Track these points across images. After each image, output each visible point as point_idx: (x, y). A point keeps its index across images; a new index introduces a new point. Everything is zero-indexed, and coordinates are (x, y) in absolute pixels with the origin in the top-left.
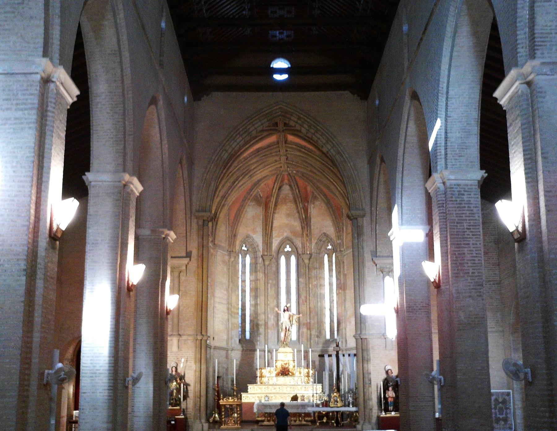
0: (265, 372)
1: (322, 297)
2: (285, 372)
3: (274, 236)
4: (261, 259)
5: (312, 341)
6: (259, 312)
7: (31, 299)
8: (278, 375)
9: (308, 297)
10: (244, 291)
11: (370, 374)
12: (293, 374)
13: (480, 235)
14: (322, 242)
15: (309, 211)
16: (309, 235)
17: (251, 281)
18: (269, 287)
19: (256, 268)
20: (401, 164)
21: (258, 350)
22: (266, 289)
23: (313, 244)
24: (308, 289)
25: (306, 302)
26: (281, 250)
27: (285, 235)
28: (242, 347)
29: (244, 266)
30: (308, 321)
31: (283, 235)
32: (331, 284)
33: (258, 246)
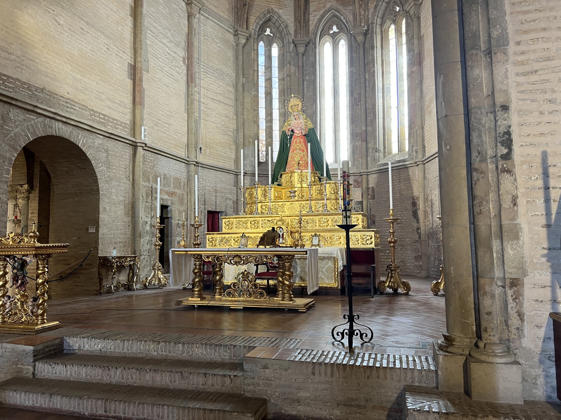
4: (292, 45)
5: (369, 158)
7: (269, 140)
9: (363, 92)
10: (269, 94)
11: (505, 108)
13: (517, 32)
17: (280, 80)
18: (305, 86)
21: (339, 176)
24: (362, 80)
29: (269, 57)
33: (287, 26)
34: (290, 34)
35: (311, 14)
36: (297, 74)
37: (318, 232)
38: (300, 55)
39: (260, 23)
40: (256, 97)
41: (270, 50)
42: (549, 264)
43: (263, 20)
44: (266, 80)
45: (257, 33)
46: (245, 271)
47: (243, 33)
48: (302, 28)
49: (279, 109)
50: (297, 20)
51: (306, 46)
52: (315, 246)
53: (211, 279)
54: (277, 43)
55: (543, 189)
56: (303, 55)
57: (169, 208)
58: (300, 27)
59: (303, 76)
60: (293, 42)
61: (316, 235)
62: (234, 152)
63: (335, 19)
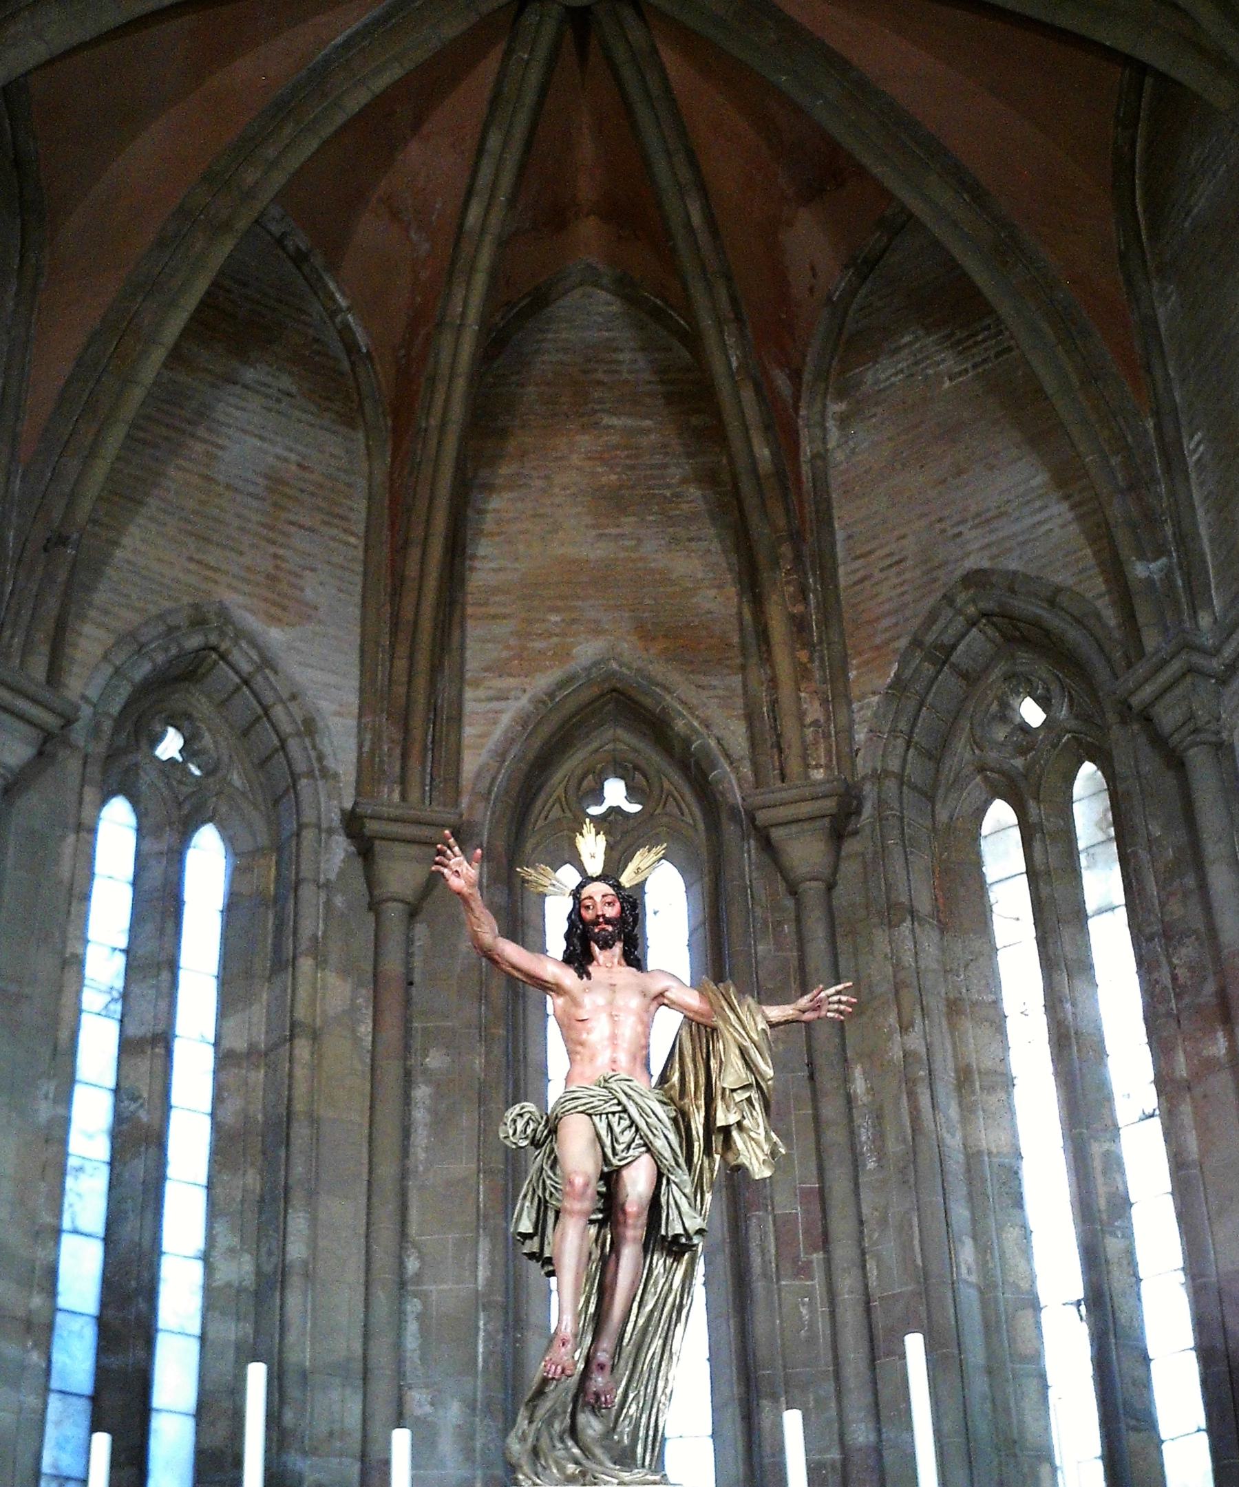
1: (999, 1186)
3: (474, 660)
4: (340, 848)
15: (807, 450)
16: (824, 630)
17: (225, 1059)
18: (420, 1115)
20: (950, 1301)
22: (387, 1133)
23: (866, 709)
25: (825, 1242)
27: (587, 651)
29: (158, 903)
30: (861, 1434)
31: (563, 654)
32: (1074, 1048)
33: (309, 727)
34: (325, 773)
35: (477, 684)
36: (365, 1029)
38: (394, 912)
40: (55, 1135)
41: (176, 857)
42: (149, 1035)
43: (160, 658)
44: (128, 1047)
45: (107, 725)
46: (544, 491)
47: (22, 704)
48: (416, 750)
49: (206, 1258)
50: (376, 698)
54: (222, 829)
55: (1090, 907)
56: (413, 913)
60: (353, 823)
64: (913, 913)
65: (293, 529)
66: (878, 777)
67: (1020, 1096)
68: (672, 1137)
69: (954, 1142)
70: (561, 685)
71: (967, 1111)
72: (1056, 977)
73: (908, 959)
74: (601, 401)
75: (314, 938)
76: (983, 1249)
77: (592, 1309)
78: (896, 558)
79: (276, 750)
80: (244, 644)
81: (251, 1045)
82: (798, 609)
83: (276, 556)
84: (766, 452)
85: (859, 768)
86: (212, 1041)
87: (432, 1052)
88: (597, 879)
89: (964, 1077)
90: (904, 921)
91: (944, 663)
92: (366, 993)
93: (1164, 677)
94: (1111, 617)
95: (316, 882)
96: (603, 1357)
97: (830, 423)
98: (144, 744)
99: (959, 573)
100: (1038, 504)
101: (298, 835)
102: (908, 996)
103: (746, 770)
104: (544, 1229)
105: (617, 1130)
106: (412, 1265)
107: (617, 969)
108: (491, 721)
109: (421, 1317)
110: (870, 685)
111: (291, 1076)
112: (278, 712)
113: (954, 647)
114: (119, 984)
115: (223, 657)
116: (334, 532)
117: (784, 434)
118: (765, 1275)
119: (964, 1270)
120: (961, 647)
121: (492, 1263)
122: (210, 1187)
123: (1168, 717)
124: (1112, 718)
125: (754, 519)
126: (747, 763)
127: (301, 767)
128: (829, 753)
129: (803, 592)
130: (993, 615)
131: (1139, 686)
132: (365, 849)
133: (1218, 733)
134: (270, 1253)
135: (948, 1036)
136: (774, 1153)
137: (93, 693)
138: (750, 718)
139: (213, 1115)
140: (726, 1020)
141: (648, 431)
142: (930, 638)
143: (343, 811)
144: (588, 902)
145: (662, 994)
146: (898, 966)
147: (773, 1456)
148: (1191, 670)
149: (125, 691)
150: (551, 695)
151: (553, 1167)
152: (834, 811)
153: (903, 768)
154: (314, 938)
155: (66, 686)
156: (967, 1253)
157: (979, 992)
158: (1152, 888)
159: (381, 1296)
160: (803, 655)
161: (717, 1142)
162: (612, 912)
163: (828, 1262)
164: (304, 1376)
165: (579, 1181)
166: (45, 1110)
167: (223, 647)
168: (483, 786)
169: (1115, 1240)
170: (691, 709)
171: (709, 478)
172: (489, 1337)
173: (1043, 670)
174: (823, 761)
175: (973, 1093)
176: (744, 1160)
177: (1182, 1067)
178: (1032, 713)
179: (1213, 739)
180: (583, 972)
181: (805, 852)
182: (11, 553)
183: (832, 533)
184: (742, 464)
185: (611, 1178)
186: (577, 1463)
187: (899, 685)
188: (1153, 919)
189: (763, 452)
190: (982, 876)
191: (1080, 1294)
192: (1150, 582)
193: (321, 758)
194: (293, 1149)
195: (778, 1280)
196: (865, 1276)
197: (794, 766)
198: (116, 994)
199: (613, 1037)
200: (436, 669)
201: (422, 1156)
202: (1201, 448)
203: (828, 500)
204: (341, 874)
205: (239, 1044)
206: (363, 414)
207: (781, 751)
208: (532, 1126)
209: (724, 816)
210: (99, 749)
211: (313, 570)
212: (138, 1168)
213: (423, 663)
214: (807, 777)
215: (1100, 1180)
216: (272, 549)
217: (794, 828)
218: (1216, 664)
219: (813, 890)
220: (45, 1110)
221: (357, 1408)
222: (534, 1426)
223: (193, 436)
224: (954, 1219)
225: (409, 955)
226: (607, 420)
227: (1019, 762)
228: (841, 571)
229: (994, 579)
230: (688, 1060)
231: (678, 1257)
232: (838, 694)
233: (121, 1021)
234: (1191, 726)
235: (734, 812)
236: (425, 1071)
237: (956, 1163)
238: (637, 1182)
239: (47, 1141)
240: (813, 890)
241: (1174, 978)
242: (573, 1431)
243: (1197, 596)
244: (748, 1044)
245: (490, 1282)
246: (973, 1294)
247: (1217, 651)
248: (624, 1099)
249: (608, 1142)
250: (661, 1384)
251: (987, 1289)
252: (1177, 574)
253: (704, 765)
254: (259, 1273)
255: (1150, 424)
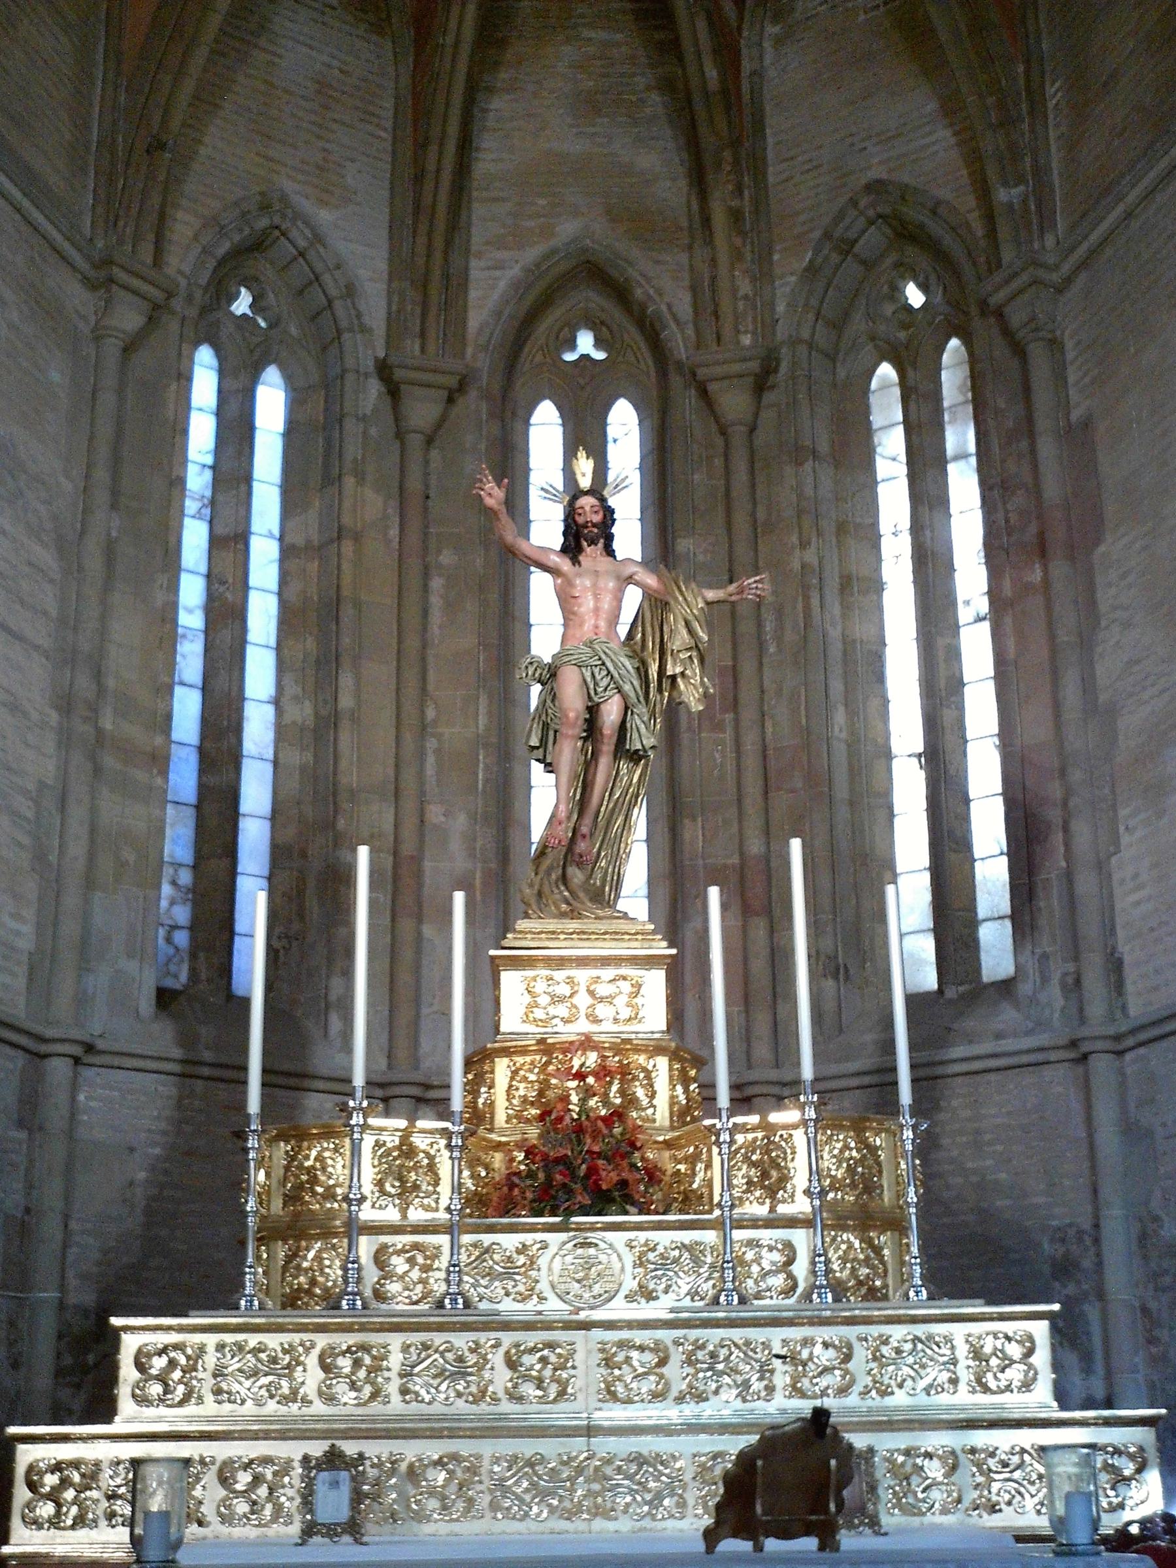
0: (355, 1163)
2: (581, 1168)
4: (374, 388)
6: (349, 776)
8: (495, 1203)
12: (689, 1201)
14: (852, 268)
15: (747, 66)
16: (754, 223)
17: (288, 552)
18: (435, 601)
19: (332, 451)
25: (735, 705)
26: (532, 354)
27: (567, 229)
28: (187, 1040)
29: (236, 429)
30: (755, 847)
32: (932, 565)
33: (350, 291)
34: (364, 330)
35: (480, 255)
36: (394, 532)
37: (347, 1435)
39: (221, 251)
42: (232, 535)
43: (237, 238)
44: (216, 542)
46: (535, 95)
47: (136, 283)
48: (433, 311)
51: (450, 400)
52: (331, 1531)
53: (918, 1260)
54: (283, 369)
56: (429, 441)
57: (579, 601)
58: (425, 305)
59: (425, 550)
60: (384, 370)
61: (333, 1459)
62: (29, 913)
63: (593, 280)
64: (814, 453)
65: (335, 126)
66: (794, 342)
67: (888, 598)
68: (636, 683)
69: (835, 633)
70: (546, 257)
71: (846, 608)
72: (920, 508)
73: (809, 491)
74: (582, 16)
75: (355, 460)
76: (852, 713)
77: (578, 797)
78: (815, 163)
79: (325, 309)
80: (299, 223)
81: (308, 541)
82: (735, 203)
83: (325, 150)
84: (714, 73)
85: (779, 334)
86: (277, 535)
87: (445, 552)
88: (587, 493)
89: (846, 583)
90: (807, 460)
91: (848, 252)
92: (394, 504)
93: (1016, 284)
94: (979, 228)
95: (357, 416)
96: (584, 830)
97: (766, 44)
98: (223, 302)
99: (863, 182)
100: (927, 129)
101: (342, 378)
102: (807, 522)
103: (690, 331)
104: (546, 743)
105: (598, 677)
106: (430, 713)
107: (600, 558)
108: (491, 286)
109: (438, 751)
110: (789, 269)
111: (339, 567)
112: (327, 278)
113: (856, 241)
114: (208, 493)
115: (283, 234)
116: (370, 128)
117: (728, 52)
118: (690, 729)
119: (836, 729)
120: (862, 242)
121: (489, 713)
122: (279, 648)
123: (1017, 317)
124: (974, 310)
125: (703, 129)
126: (691, 326)
127: (344, 324)
128: (755, 321)
129: (739, 190)
130: (887, 217)
131: (997, 290)
132: (393, 391)
133: (1053, 331)
134: (325, 702)
135: (836, 550)
136: (706, 695)
137: (187, 269)
138: (694, 289)
139: (280, 594)
140: (676, 599)
141: (618, 44)
142: (837, 235)
143: (376, 359)
144: (580, 511)
145: (631, 577)
146: (800, 496)
147: (691, 859)
148: (1034, 282)
149: (211, 264)
150: (538, 265)
151: (553, 701)
152: (758, 370)
153: (813, 335)
154: (355, 460)
155: (167, 263)
156: (840, 717)
157: (861, 516)
158: (996, 449)
159: (408, 737)
160: (738, 241)
161: (666, 684)
162: (597, 518)
163: (737, 721)
164: (353, 794)
165: (572, 715)
166: (160, 598)
167: (283, 227)
168: (482, 341)
169: (950, 712)
170: (648, 280)
171: (667, 86)
172: (486, 766)
173: (923, 261)
174: (750, 327)
175: (852, 595)
176: (684, 698)
177: (1007, 589)
178: (915, 296)
179: (1050, 336)
180: (575, 561)
181: (734, 402)
182: (120, 154)
183: (764, 138)
184: (695, 82)
185: (593, 711)
186: (568, 903)
187: (811, 270)
188: (994, 472)
189: (712, 73)
190: (869, 423)
191: (920, 749)
192: (1010, 205)
193: (359, 316)
194: (342, 625)
195: (699, 733)
196: (763, 732)
197: (727, 331)
198: (206, 501)
199: (596, 610)
200: (448, 243)
201: (436, 631)
202: (1060, 94)
203: (762, 110)
204: (376, 410)
205: (298, 540)
206: (391, 24)
207: (717, 318)
208: (539, 671)
209: (671, 368)
210: (192, 312)
211: (353, 161)
212: (225, 636)
213: (439, 242)
214: (738, 342)
215: (942, 666)
216: (321, 144)
217: (726, 383)
218: (1055, 277)
219: (738, 434)
220: (160, 598)
221: (391, 818)
222: (539, 877)
223: (256, 46)
224: (831, 692)
225: (426, 474)
226: (586, 33)
227: (902, 335)
228: (771, 169)
229: (890, 188)
230: (648, 625)
231: (637, 763)
232: (763, 274)
233: (211, 522)
234: (1033, 326)
235: (679, 365)
236: (440, 566)
237: (836, 650)
238: (611, 712)
239: (163, 620)
240: (738, 434)
241: (1007, 521)
242: (564, 879)
243: (1046, 222)
244: (690, 618)
245: (487, 729)
246: (843, 747)
247: (1057, 267)
248: (603, 657)
249: (592, 686)
250: (622, 845)
251: (853, 745)
252: (1032, 198)
253: (657, 325)
254: (316, 714)
255: (1021, 69)
